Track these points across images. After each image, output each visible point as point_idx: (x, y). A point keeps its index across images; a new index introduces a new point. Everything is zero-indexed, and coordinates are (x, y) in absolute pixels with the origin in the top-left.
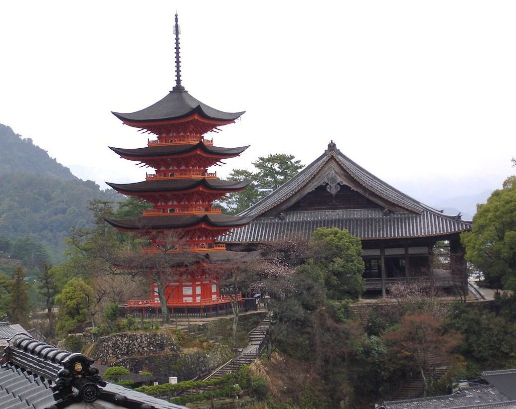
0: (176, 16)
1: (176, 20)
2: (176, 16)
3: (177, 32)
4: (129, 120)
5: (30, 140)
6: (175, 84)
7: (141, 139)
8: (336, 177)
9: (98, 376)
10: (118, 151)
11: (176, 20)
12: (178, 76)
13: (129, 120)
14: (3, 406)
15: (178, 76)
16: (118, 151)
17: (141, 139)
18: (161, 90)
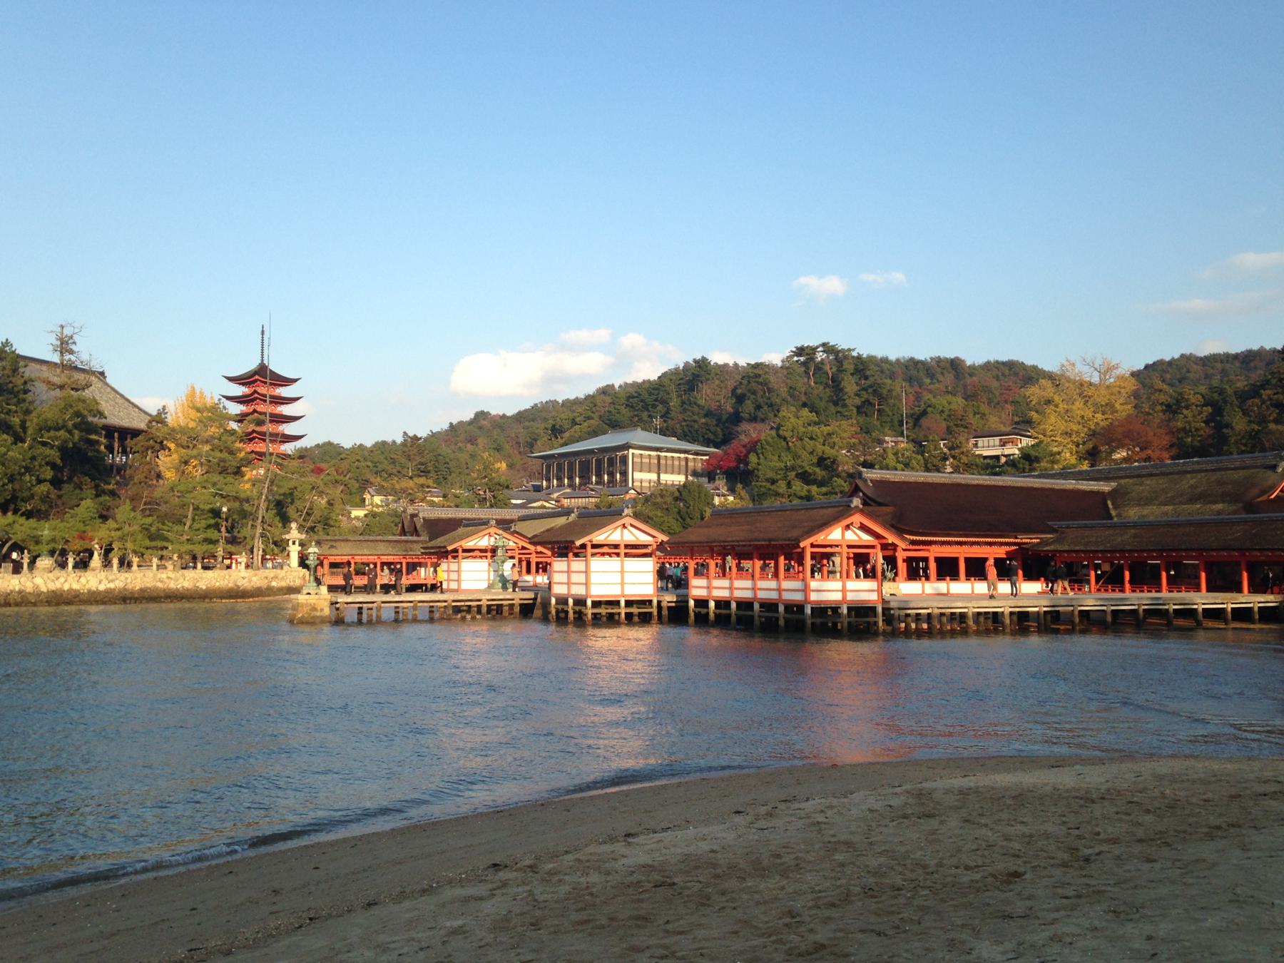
3: (263, 333)
4: (231, 379)
13: (231, 379)
18: (250, 365)
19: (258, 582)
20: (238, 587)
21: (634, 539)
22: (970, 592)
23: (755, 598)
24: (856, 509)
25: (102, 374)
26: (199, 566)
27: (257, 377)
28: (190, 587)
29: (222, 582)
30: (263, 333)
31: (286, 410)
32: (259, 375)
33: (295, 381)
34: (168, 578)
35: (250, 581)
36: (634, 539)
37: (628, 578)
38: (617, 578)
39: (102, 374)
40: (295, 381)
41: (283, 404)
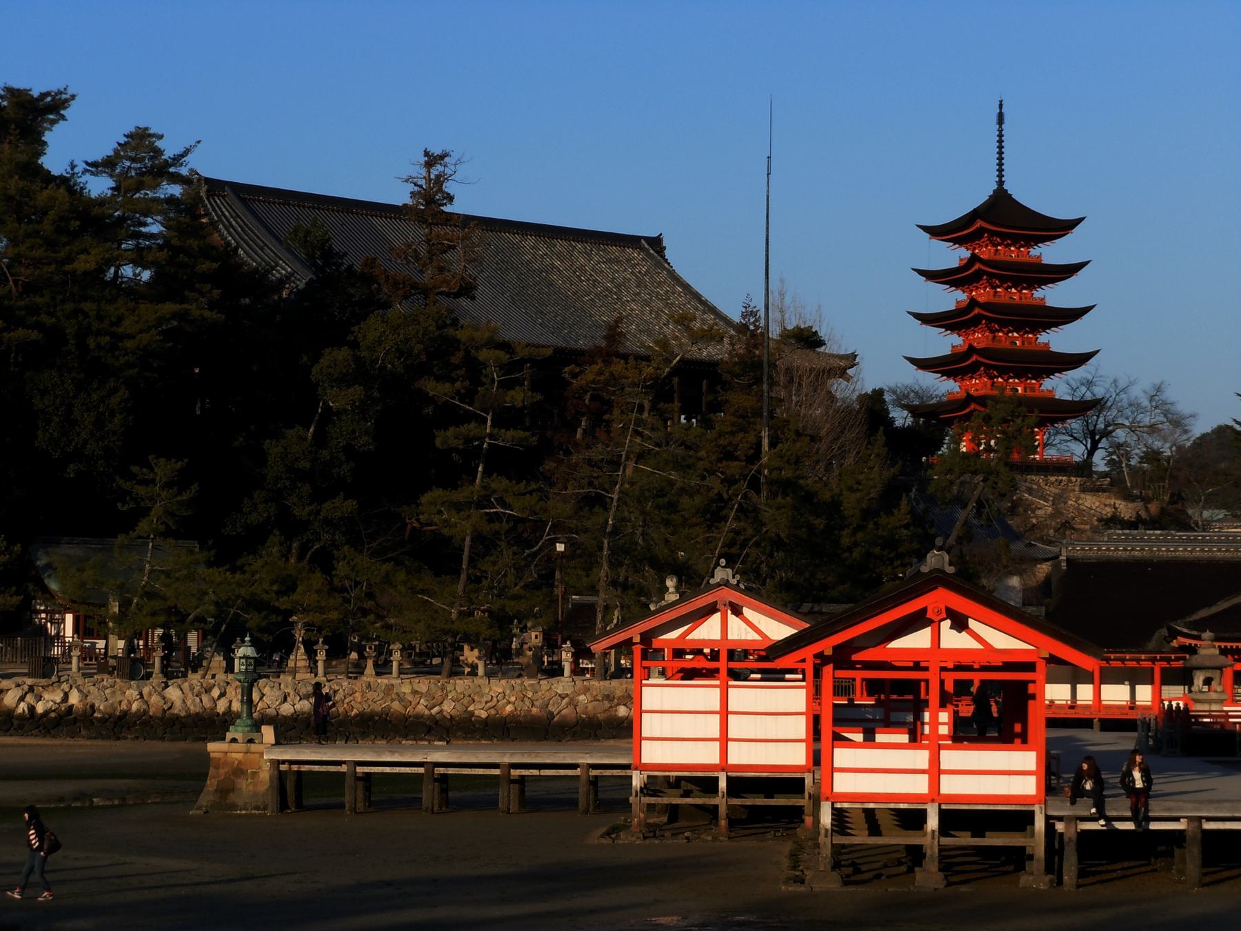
0: (1001, 101)
1: (1001, 106)
2: (1001, 101)
3: (1001, 119)
4: (936, 232)
5: (960, 632)
6: (995, 187)
7: (951, 256)
8: (477, 757)
9: (445, 261)
10: (917, 316)
11: (1001, 106)
12: (1001, 176)
13: (936, 232)
14: (5, 746)
15: (1001, 176)
16: (917, 316)
17: (951, 256)
18: (979, 195)
19: (590, 706)
20: (552, 715)
21: (757, 637)
22: (926, 776)
23: (724, 766)
24: (937, 580)
25: (656, 243)
26: (19, 660)
27: (979, 223)
28: (454, 713)
29: (519, 704)
30: (1001, 119)
31: (1055, 295)
32: (983, 219)
33: (1078, 221)
34: (415, 692)
35: (573, 703)
36: (757, 637)
37: (737, 727)
38: (712, 726)
39: (656, 243)
40: (1078, 221)
41: (1054, 281)
